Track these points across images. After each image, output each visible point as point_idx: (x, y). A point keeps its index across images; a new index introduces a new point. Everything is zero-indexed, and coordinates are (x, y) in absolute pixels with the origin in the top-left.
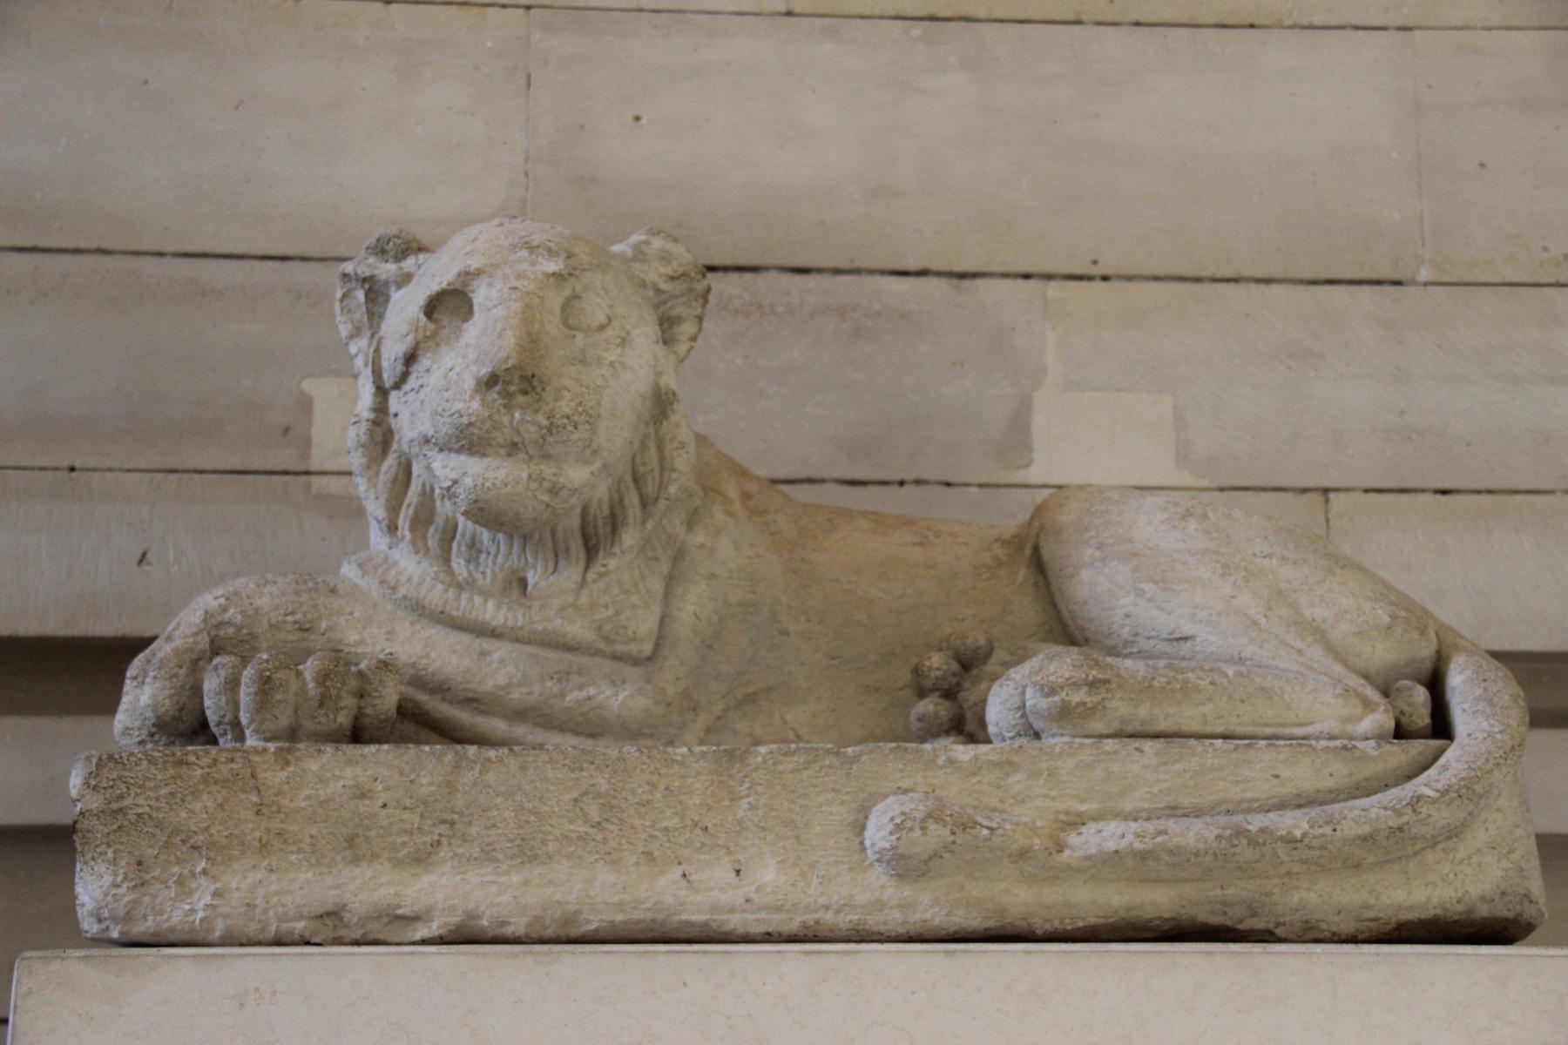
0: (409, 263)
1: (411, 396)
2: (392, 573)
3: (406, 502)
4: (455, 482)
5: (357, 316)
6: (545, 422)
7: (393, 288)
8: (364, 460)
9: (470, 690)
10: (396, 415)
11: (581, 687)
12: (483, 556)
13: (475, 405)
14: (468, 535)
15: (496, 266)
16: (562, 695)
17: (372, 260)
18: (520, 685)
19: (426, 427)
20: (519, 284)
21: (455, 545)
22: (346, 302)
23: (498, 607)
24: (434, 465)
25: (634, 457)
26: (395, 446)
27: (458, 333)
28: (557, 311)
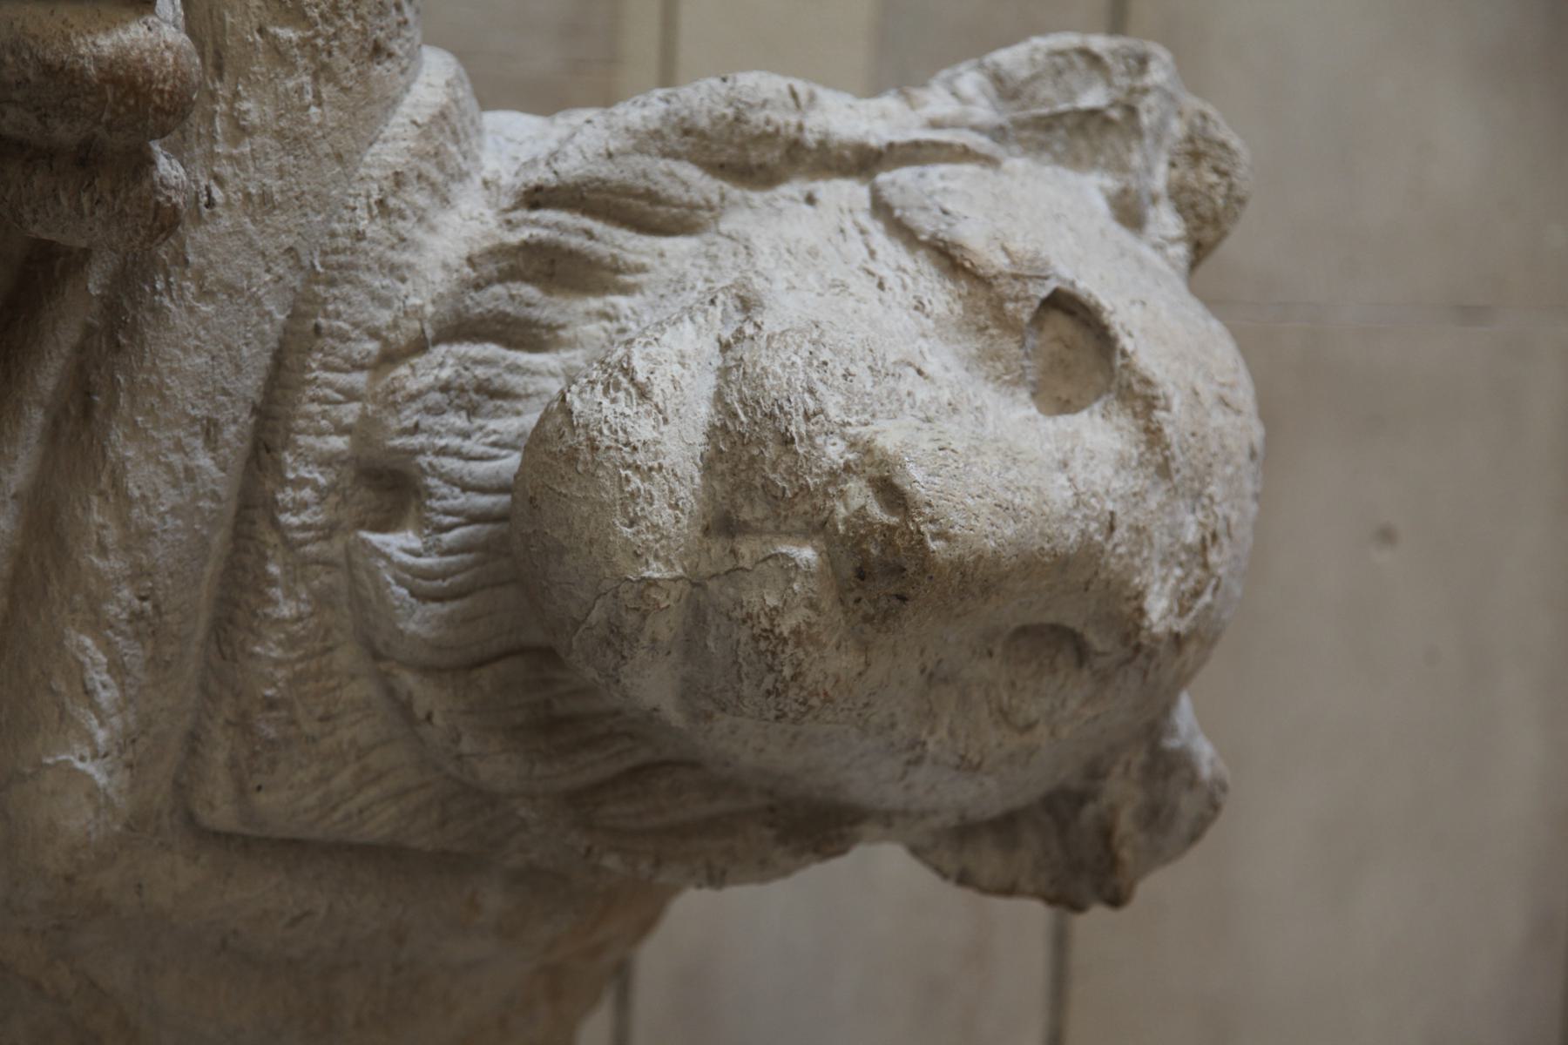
0: (1166, 221)
1: (856, 248)
2: (421, 199)
3: (597, 227)
4: (643, 394)
5: (1046, 91)
6: (785, 626)
7: (1111, 183)
8: (704, 122)
9: (113, 406)
10: (810, 200)
11: (117, 668)
12: (460, 421)
13: (835, 452)
14: (514, 381)
15: (1164, 471)
16: (97, 625)
17: (1177, 128)
18: (124, 523)
19: (788, 305)
20: (1121, 533)
21: (490, 349)
22: (1081, 63)
23: (327, 461)
24: (687, 328)
25: (695, 765)
26: (735, 193)
27: (1010, 380)
28: (1050, 617)
